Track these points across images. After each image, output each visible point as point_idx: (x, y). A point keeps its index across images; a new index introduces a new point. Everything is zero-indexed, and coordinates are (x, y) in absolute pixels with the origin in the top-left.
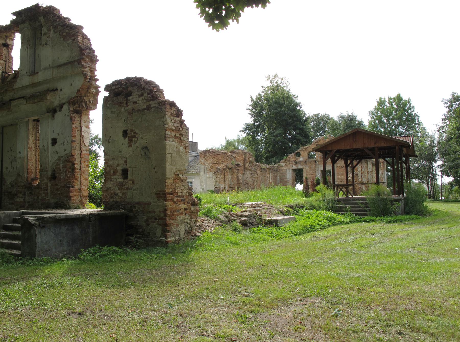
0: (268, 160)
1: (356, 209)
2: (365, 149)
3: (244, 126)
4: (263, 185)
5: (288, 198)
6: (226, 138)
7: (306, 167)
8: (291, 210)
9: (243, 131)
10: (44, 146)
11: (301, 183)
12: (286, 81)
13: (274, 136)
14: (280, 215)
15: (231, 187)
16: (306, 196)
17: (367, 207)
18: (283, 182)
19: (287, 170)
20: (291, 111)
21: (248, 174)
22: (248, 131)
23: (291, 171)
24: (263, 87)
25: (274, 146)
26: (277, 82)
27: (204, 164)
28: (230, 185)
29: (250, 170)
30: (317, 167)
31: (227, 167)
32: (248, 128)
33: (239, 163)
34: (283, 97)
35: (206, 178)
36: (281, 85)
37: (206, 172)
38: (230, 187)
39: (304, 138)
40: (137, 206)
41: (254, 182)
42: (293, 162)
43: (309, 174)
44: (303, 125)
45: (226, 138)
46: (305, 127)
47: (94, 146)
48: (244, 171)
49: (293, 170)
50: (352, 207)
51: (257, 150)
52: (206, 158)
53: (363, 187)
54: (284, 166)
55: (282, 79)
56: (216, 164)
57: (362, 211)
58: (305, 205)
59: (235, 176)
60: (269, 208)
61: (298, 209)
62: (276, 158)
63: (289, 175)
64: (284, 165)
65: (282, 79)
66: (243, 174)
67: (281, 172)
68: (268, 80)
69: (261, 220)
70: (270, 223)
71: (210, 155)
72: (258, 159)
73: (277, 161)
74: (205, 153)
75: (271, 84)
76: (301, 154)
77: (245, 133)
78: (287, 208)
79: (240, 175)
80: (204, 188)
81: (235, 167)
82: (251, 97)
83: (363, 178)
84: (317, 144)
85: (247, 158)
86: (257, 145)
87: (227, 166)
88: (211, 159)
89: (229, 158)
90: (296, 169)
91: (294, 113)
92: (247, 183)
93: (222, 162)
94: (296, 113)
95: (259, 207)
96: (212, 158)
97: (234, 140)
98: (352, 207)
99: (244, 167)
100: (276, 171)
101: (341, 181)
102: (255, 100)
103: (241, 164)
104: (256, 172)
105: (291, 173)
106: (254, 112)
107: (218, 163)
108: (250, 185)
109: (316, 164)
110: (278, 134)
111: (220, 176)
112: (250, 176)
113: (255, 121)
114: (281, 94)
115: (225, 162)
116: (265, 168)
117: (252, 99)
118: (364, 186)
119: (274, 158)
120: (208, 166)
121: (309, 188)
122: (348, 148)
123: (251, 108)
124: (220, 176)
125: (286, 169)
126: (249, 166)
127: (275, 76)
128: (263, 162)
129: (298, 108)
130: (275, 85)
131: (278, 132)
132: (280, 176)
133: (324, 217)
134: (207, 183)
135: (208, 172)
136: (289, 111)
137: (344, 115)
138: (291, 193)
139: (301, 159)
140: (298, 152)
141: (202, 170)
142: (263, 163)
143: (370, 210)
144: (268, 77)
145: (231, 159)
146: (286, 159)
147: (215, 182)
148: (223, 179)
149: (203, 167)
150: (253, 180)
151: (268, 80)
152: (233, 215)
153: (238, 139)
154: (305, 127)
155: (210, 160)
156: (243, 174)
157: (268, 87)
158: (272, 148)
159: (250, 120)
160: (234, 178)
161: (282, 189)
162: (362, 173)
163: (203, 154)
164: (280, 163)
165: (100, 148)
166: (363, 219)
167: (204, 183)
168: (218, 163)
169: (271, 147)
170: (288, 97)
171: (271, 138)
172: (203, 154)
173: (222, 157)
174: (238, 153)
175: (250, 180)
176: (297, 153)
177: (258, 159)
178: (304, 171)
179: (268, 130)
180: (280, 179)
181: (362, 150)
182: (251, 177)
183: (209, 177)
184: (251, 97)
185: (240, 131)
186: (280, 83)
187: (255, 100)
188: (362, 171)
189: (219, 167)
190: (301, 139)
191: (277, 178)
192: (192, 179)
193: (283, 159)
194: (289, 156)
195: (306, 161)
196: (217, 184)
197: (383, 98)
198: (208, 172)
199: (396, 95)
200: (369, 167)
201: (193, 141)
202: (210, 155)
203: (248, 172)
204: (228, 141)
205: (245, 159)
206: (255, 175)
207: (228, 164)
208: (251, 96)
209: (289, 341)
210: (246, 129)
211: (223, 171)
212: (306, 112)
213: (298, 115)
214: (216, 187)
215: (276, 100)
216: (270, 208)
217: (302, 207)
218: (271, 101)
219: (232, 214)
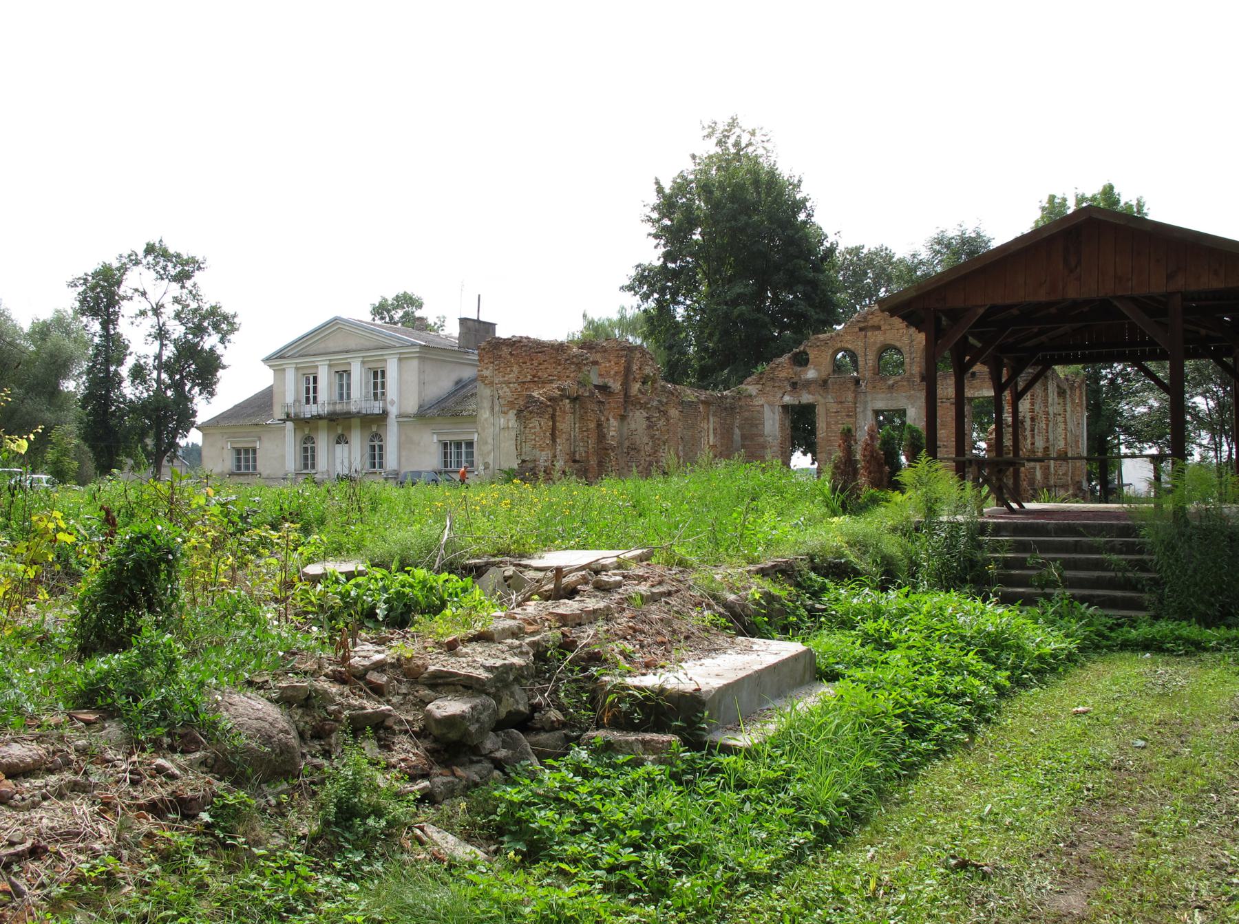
0: (705, 376)
1: (1119, 593)
2: (1116, 303)
3: (633, 273)
4: (668, 457)
5: (769, 516)
6: (585, 316)
8: (781, 591)
9: (630, 288)
11: (810, 448)
12: (765, 139)
13: (726, 304)
14: (721, 640)
15: (578, 462)
16: (845, 509)
17: (1142, 566)
18: (753, 450)
19: (766, 408)
20: (779, 227)
21: (638, 420)
22: (645, 287)
23: (778, 410)
24: (694, 157)
25: (726, 333)
26: (737, 144)
27: (492, 383)
28: (575, 452)
29: (643, 406)
31: (564, 395)
32: (645, 280)
33: (611, 383)
34: (756, 182)
35: (497, 429)
36: (750, 149)
37: (497, 408)
38: (575, 461)
39: (818, 310)
41: (657, 444)
42: (786, 383)
43: (837, 423)
44: (817, 268)
45: (585, 316)
46: (821, 277)
47: (206, 338)
48: (625, 408)
49: (785, 408)
50: (1067, 565)
51: (673, 346)
53: (1034, 468)
54: (756, 397)
55: (753, 134)
57: (1111, 584)
58: (852, 558)
59: (592, 426)
60: (662, 594)
61: (820, 579)
62: (730, 371)
63: (772, 424)
64: (754, 393)
65: (753, 134)
66: (623, 418)
68: (709, 136)
69: (594, 694)
70: (648, 716)
72: (675, 372)
73: (733, 379)
74: (495, 349)
75: (719, 150)
76: (811, 356)
77: (636, 293)
78: (768, 586)
79: (612, 420)
80: (491, 463)
81: (592, 394)
82: (657, 183)
83: (1036, 437)
84: (862, 325)
85: (635, 368)
86: (672, 331)
87: (562, 390)
88: (516, 369)
89: (573, 363)
90: (793, 406)
91: (790, 232)
92: (633, 448)
94: (797, 233)
95: (604, 588)
96: (518, 363)
97: (609, 320)
98: (1067, 565)
99: (626, 394)
100: (731, 410)
102: (667, 191)
103: (616, 386)
104: (665, 413)
105: (777, 418)
106: (665, 229)
107: (537, 381)
108: (642, 453)
109: (859, 390)
110: (739, 295)
111: (538, 424)
112: (645, 424)
113: (668, 256)
114: (749, 171)
115: (559, 377)
116: (695, 400)
117: (660, 190)
118: (1038, 465)
119: (726, 372)
121: (855, 472)
122: (1042, 296)
123: (655, 215)
124: (538, 424)
126: (642, 393)
127: (733, 123)
128: (690, 382)
129: (802, 217)
130: (733, 150)
131: (738, 289)
132: (741, 428)
133: (963, 638)
134: (502, 445)
136: (774, 226)
137: (950, 234)
138: (780, 492)
139: (811, 374)
140: (800, 352)
142: (691, 385)
143: (1156, 583)
144: (710, 127)
145: (580, 368)
146: (761, 373)
147: (519, 442)
148: (548, 434)
149: (487, 392)
150: (652, 437)
151: (709, 136)
152: (374, 677)
153: (623, 317)
154: (821, 277)
155: (512, 371)
156: (623, 418)
157: (710, 157)
158: (720, 341)
159: (652, 254)
160: (587, 430)
161: (747, 475)
162: (1033, 419)
163: (489, 351)
164: (743, 386)
165: (223, 343)
166: (1143, 631)
167: (490, 447)
168: (536, 379)
169: (715, 338)
170: (773, 182)
171: (715, 310)
172: (489, 351)
174: (605, 351)
175: (643, 439)
176: (796, 354)
177: (675, 372)
178: (820, 411)
179: (709, 285)
180: (744, 437)
181: (1104, 308)
182: (649, 427)
184: (657, 183)
185: (622, 288)
186: (747, 146)
187: (667, 191)
188: (1032, 411)
189: (535, 394)
190: (812, 312)
191: (733, 434)
192: (473, 432)
193: (753, 373)
194: (772, 365)
195: (825, 382)
196: (527, 448)
197: (1059, 195)
198: (505, 409)
199: (1101, 189)
200: (1050, 400)
201: (481, 319)
202: (511, 354)
203: (638, 413)
204: (591, 322)
205: (628, 370)
206: (662, 423)
207: (567, 383)
208: (656, 179)
210: (640, 283)
211: (548, 406)
212: (826, 230)
213: (800, 238)
214: (523, 461)
215: (733, 190)
216: (669, 594)
217: (840, 571)
218: (717, 194)
219: (367, 669)
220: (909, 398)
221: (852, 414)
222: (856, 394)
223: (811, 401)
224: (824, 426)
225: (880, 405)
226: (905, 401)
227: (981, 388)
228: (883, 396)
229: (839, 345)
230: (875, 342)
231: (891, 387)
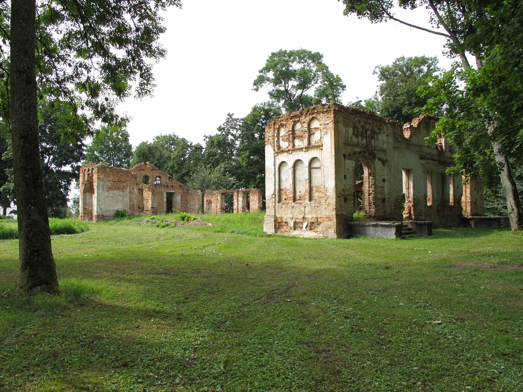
37: (105, 189)
38: (139, 208)
40: (407, 378)
56: (118, 183)
71: (110, 171)
89: (133, 177)
96: (113, 175)
120: (108, 184)
129: (118, 45)
198: (108, 190)
202: (110, 171)
209: (392, 391)
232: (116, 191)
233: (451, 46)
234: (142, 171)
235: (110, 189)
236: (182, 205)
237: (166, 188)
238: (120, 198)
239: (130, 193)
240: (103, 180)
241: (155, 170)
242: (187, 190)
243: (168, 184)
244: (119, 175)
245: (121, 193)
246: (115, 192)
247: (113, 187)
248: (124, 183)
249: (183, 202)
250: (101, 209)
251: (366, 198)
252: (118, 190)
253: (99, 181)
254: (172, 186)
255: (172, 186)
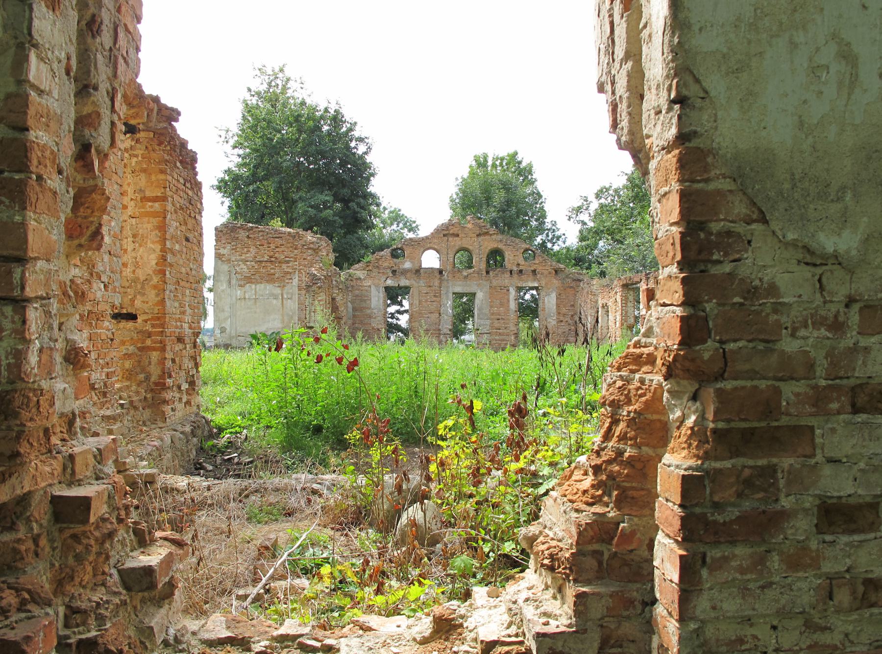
7: (418, 283)
10: (740, 14)
19: (373, 287)
24: (249, 90)
30: (444, 284)
35: (234, 298)
37: (234, 282)
42: (388, 271)
43: (426, 301)
52: (236, 245)
67: (357, 292)
74: (232, 232)
88: (253, 250)
93: (287, 259)
101: (498, 319)
109: (443, 278)
125: (370, 286)
135: (242, 283)
141: (222, 278)
146: (369, 262)
155: (249, 251)
163: (227, 233)
168: (273, 259)
172: (227, 233)
173: (289, 245)
183: (245, 298)
198: (242, 283)
202: (248, 237)
220: (479, 285)
221: (438, 295)
222: (441, 281)
223: (408, 284)
224: (418, 303)
225: (458, 289)
226: (476, 287)
227: (527, 281)
228: (460, 283)
229: (428, 245)
230: (454, 245)
231: (466, 277)
232: (262, 286)
233: (818, 643)
234: (451, 239)
235: (249, 280)
236: (562, 318)
237: (515, 276)
238: (275, 302)
239: (299, 290)
240: (229, 261)
241: (486, 233)
242: (574, 280)
243: (521, 268)
244: (272, 246)
245: (278, 291)
246: (260, 287)
247: (257, 277)
248: (284, 266)
249: (564, 310)
250: (223, 330)
251: (515, 616)
252: (268, 281)
253: (220, 262)
254: (534, 271)
255: (534, 271)
